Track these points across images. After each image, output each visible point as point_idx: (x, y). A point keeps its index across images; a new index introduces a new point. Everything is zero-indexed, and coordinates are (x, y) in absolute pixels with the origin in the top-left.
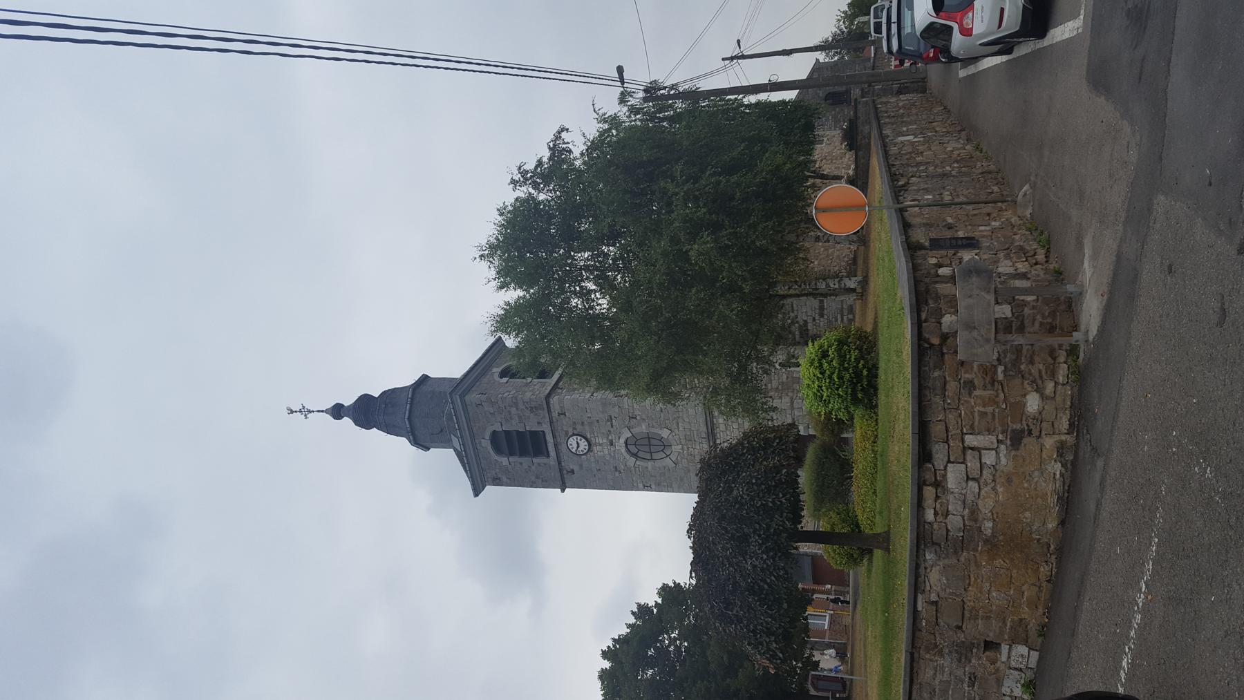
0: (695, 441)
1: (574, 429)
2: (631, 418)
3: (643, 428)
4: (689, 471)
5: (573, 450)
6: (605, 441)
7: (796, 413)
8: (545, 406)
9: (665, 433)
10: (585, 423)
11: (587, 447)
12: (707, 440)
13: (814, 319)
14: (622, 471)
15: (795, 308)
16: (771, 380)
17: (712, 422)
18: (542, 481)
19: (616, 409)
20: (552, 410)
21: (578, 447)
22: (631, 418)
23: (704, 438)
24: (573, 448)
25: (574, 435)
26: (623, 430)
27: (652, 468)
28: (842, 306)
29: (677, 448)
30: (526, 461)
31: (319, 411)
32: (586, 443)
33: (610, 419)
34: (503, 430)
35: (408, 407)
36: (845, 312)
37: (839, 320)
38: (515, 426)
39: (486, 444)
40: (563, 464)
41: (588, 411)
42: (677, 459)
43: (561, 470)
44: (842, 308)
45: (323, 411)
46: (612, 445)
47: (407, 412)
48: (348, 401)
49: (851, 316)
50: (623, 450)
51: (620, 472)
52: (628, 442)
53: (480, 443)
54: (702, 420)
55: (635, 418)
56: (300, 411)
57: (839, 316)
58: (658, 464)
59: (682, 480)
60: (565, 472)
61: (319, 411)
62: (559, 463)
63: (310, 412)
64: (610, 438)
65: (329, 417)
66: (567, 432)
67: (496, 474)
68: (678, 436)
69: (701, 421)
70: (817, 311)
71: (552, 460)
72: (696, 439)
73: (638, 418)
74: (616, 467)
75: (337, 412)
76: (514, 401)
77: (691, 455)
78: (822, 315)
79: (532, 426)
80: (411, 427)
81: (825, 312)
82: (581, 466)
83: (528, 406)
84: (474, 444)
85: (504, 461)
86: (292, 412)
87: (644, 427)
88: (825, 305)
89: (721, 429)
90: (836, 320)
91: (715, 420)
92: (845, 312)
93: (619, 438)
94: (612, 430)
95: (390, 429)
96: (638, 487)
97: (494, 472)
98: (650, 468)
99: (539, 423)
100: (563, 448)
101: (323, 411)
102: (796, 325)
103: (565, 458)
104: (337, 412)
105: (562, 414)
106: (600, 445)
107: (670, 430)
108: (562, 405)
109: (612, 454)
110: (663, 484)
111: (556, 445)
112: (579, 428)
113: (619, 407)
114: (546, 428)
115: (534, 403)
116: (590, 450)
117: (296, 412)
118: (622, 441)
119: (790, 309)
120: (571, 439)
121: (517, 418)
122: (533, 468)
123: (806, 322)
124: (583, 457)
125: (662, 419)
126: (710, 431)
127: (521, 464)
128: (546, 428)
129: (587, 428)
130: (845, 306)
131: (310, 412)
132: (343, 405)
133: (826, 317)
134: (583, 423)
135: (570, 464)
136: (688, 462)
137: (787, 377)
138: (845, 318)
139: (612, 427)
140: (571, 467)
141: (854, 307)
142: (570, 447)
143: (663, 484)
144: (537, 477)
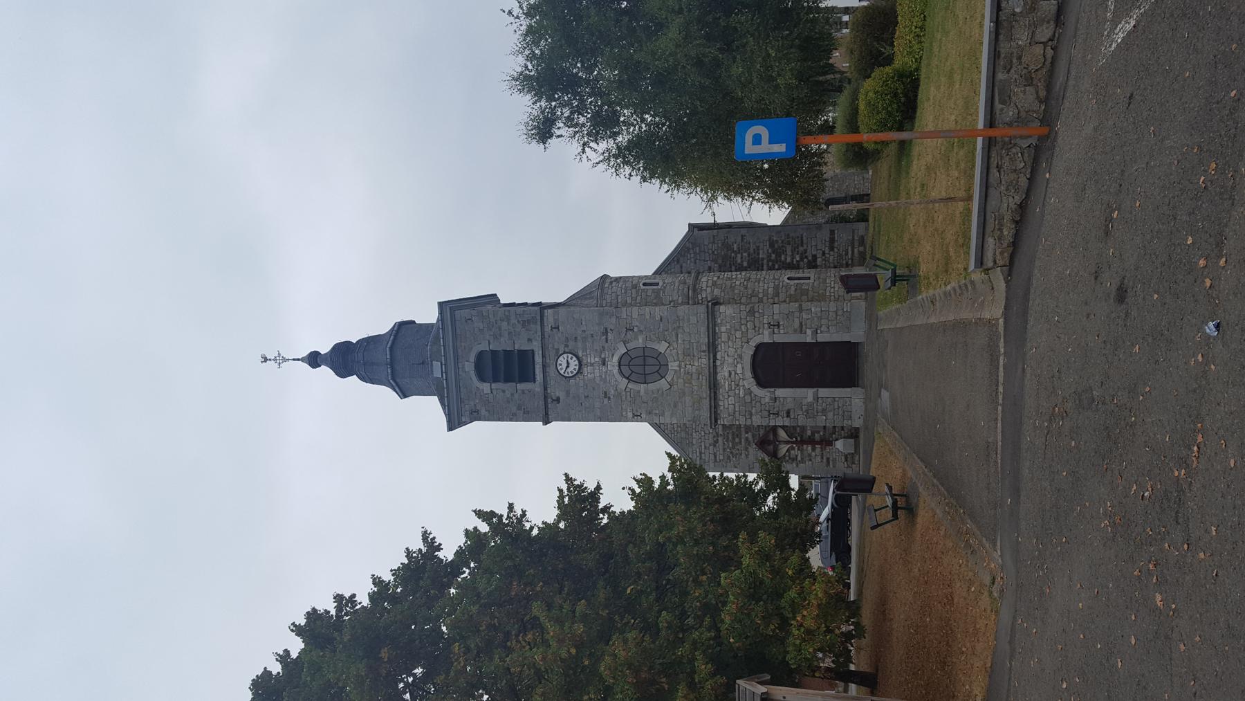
0: (694, 356)
1: (567, 346)
2: (628, 330)
3: (640, 342)
4: (684, 394)
5: (562, 372)
6: (597, 359)
7: (805, 316)
8: (539, 318)
9: (662, 347)
10: (579, 338)
11: (577, 368)
12: (707, 354)
13: (824, 254)
14: (612, 397)
15: (805, 241)
16: (779, 293)
17: (714, 331)
18: (524, 413)
19: (614, 320)
20: (546, 324)
21: (568, 367)
22: (628, 330)
23: (704, 351)
24: (562, 369)
25: (565, 353)
26: (618, 345)
27: (645, 393)
28: (853, 236)
29: (673, 365)
30: (509, 387)
31: (294, 360)
32: (577, 362)
33: (606, 333)
34: (491, 350)
35: (389, 372)
36: (856, 244)
37: (850, 253)
38: (503, 345)
39: (469, 367)
40: (549, 391)
41: (584, 323)
42: (672, 379)
43: (546, 398)
44: (853, 239)
45: (298, 360)
46: (604, 364)
47: (390, 342)
48: (324, 349)
49: (861, 249)
50: (616, 371)
51: (609, 398)
52: (622, 363)
53: (463, 367)
54: (703, 329)
55: (633, 330)
56: (275, 360)
57: (850, 249)
58: (652, 386)
59: (675, 406)
60: (550, 400)
61: (294, 360)
62: (545, 389)
63: (285, 360)
64: (603, 356)
65: (307, 366)
66: (557, 350)
67: (475, 405)
68: (675, 350)
69: (702, 331)
70: (827, 244)
71: (537, 387)
72: (695, 354)
73: (636, 330)
74: (605, 392)
75: (314, 360)
76: (506, 313)
77: (688, 373)
78: (832, 249)
79: (521, 345)
80: (391, 359)
81: (836, 245)
82: (568, 393)
83: (520, 320)
84: (457, 368)
85: (486, 387)
86: (266, 360)
87: (640, 341)
88: (836, 236)
89: (723, 340)
90: (847, 254)
91: (717, 328)
92: (856, 244)
93: (613, 355)
94: (606, 346)
95: (369, 377)
96: (626, 417)
97: (472, 403)
98: (642, 393)
99: (529, 340)
100: (551, 370)
101: (298, 360)
102: (805, 260)
103: (552, 382)
104: (314, 360)
105: (555, 328)
106: (592, 365)
107: (668, 343)
108: (556, 317)
109: (603, 376)
110: (654, 412)
111: (544, 366)
112: (571, 344)
113: (617, 317)
114: (536, 346)
115: (527, 316)
116: (580, 372)
117: (270, 360)
118: (616, 359)
119: (800, 242)
120: (561, 358)
121: (507, 335)
122: (516, 396)
123: (815, 257)
124: (572, 381)
125: (661, 330)
126: (711, 341)
127: (504, 391)
128: (536, 346)
129: (580, 344)
130: (856, 238)
131: (285, 360)
132: (351, 343)
133: (836, 250)
134: (576, 338)
135: (556, 391)
136: (685, 383)
137: (796, 290)
138: (856, 250)
139: (607, 341)
140: (557, 395)
141: (865, 238)
142: (559, 368)
143: (654, 412)
144: (519, 408)
